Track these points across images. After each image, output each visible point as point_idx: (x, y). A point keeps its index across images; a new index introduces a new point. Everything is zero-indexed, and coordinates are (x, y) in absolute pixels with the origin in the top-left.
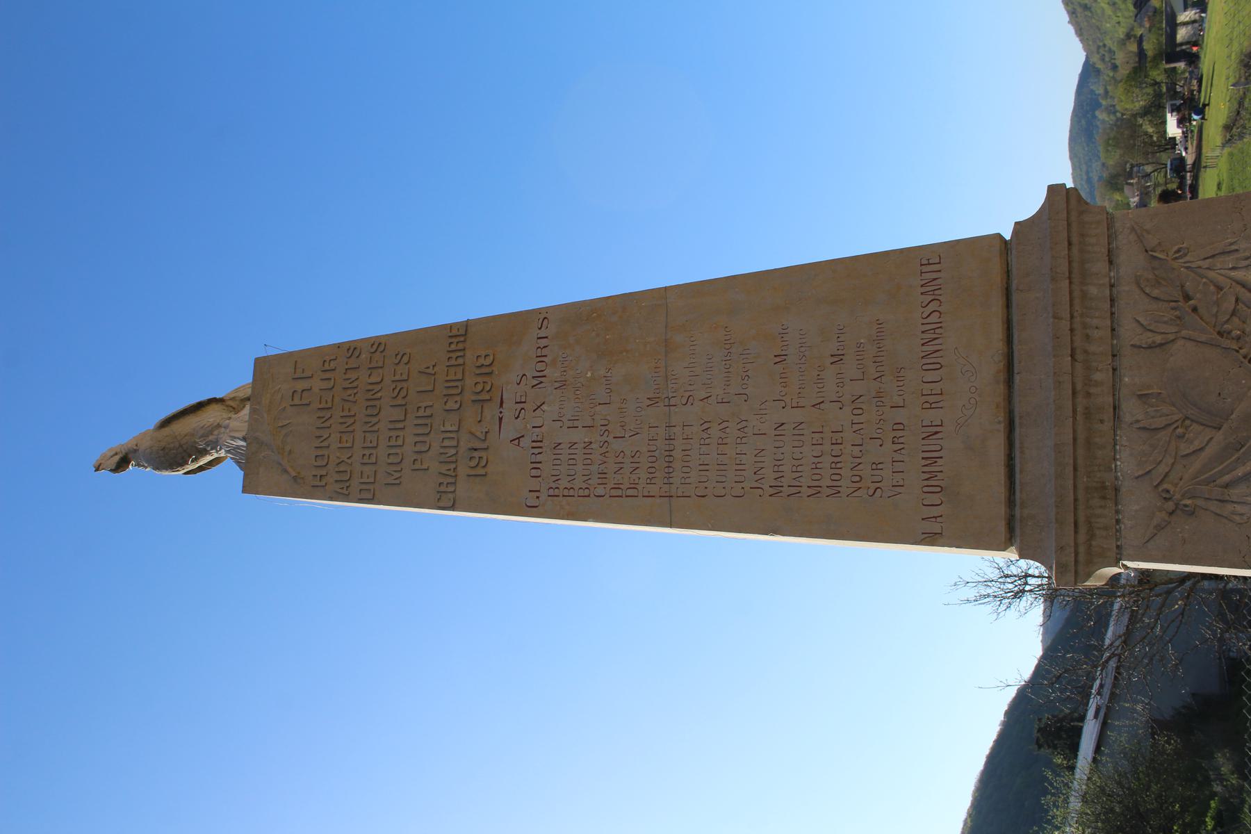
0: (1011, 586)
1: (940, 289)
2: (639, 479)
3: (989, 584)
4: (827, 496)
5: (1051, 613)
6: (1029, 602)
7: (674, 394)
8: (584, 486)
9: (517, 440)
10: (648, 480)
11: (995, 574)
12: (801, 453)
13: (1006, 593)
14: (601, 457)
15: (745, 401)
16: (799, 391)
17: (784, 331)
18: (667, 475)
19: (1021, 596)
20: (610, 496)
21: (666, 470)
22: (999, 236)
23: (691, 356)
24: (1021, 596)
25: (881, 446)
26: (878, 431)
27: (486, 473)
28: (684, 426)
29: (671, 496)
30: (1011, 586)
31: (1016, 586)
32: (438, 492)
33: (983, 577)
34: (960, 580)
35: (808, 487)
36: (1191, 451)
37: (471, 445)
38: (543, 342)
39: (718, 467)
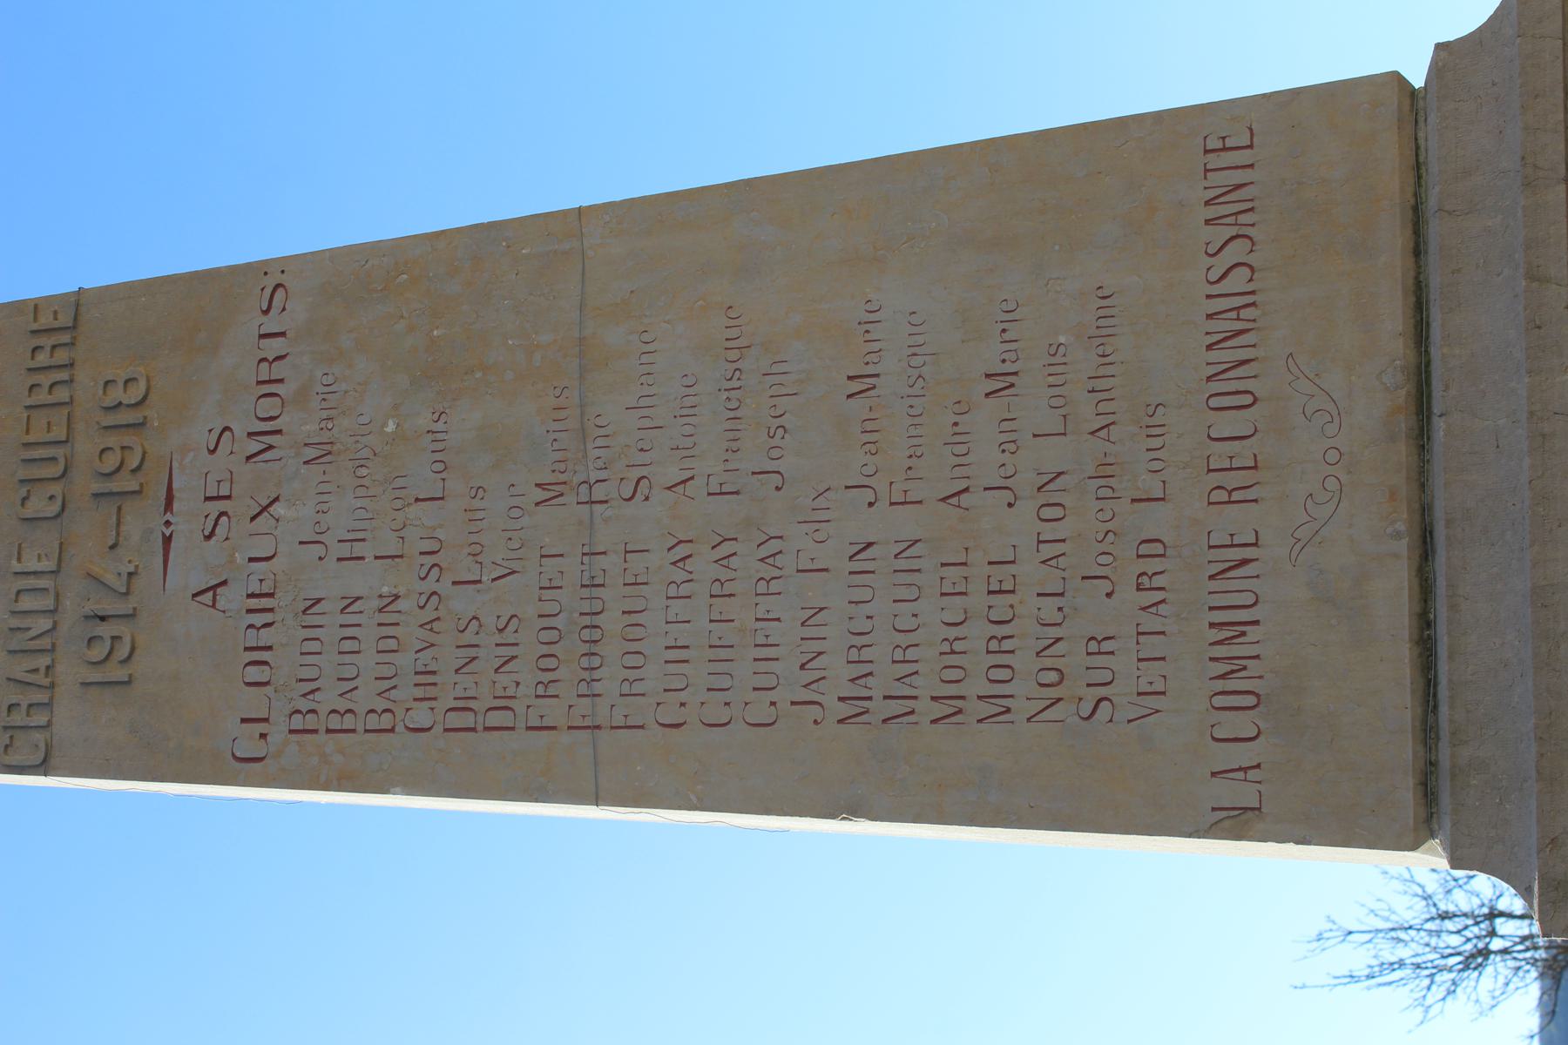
0: (1455, 940)
1: (1251, 209)
2: (518, 684)
3: (1402, 935)
4: (979, 721)
5: (1555, 1005)
6: (1501, 980)
7: (602, 475)
8: (380, 704)
9: (211, 594)
10: (541, 688)
11: (1414, 911)
12: (915, 615)
13: (1443, 957)
14: (422, 633)
15: (778, 489)
16: (910, 462)
17: (872, 317)
18: (586, 675)
19: (1480, 965)
20: (446, 730)
21: (585, 662)
22: (1397, 79)
23: (643, 379)
24: (1480, 965)
25: (1109, 595)
26: (1103, 559)
27: (130, 676)
28: (626, 552)
29: (598, 727)
30: (1455, 940)
31: (1468, 940)
32: (6, 728)
33: (1387, 919)
34: (1330, 926)
35: (933, 698)
36: (268, 416)
37: (91, 607)
38: (274, 347)
39: (713, 654)
